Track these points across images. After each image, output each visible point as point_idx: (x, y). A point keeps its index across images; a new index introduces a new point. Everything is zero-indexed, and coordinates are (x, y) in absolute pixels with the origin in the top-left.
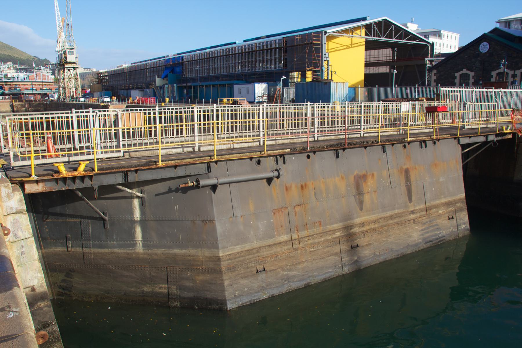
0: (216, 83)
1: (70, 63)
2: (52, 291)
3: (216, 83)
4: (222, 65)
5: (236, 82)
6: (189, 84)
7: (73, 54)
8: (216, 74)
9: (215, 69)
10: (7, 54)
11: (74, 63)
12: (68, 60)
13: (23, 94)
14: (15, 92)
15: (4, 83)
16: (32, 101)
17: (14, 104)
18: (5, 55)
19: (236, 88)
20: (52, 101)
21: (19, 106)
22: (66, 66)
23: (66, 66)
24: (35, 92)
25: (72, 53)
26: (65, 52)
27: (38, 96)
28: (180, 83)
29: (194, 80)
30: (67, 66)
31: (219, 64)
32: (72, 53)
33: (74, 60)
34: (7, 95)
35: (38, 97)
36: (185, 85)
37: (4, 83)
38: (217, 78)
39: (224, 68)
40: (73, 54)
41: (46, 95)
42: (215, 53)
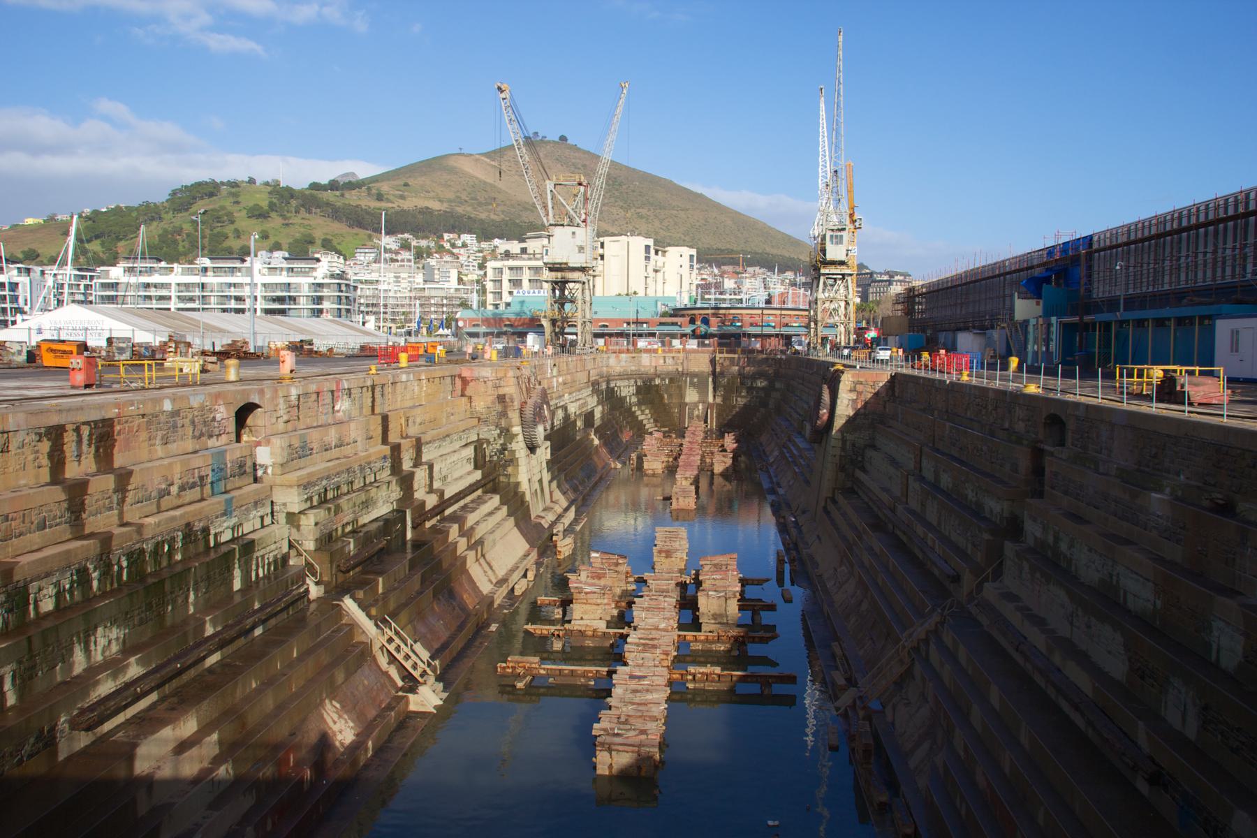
0: (1165, 312)
1: (833, 263)
2: (1010, 273)
3: (1165, 312)
4: (1228, 252)
5: (1226, 308)
6: (1087, 318)
7: (841, 243)
8: (1228, 280)
9: (1179, 268)
10: (787, 255)
11: (842, 263)
12: (829, 257)
13: (744, 335)
14: (732, 329)
15: (710, 312)
16: (752, 351)
17: (718, 356)
18: (783, 257)
19: (1223, 328)
20: (797, 352)
21: (727, 363)
22: (822, 271)
23: (822, 271)
24: (767, 331)
25: (839, 240)
26: (824, 238)
27: (774, 341)
28: (1066, 315)
29: (1112, 304)
30: (827, 271)
31: (1210, 249)
32: (839, 240)
33: (843, 258)
34: (712, 336)
35: (773, 344)
36: (1076, 319)
37: (710, 312)
38: (1178, 297)
39: (1205, 266)
40: (841, 243)
41: (788, 339)
42: (1189, 217)
